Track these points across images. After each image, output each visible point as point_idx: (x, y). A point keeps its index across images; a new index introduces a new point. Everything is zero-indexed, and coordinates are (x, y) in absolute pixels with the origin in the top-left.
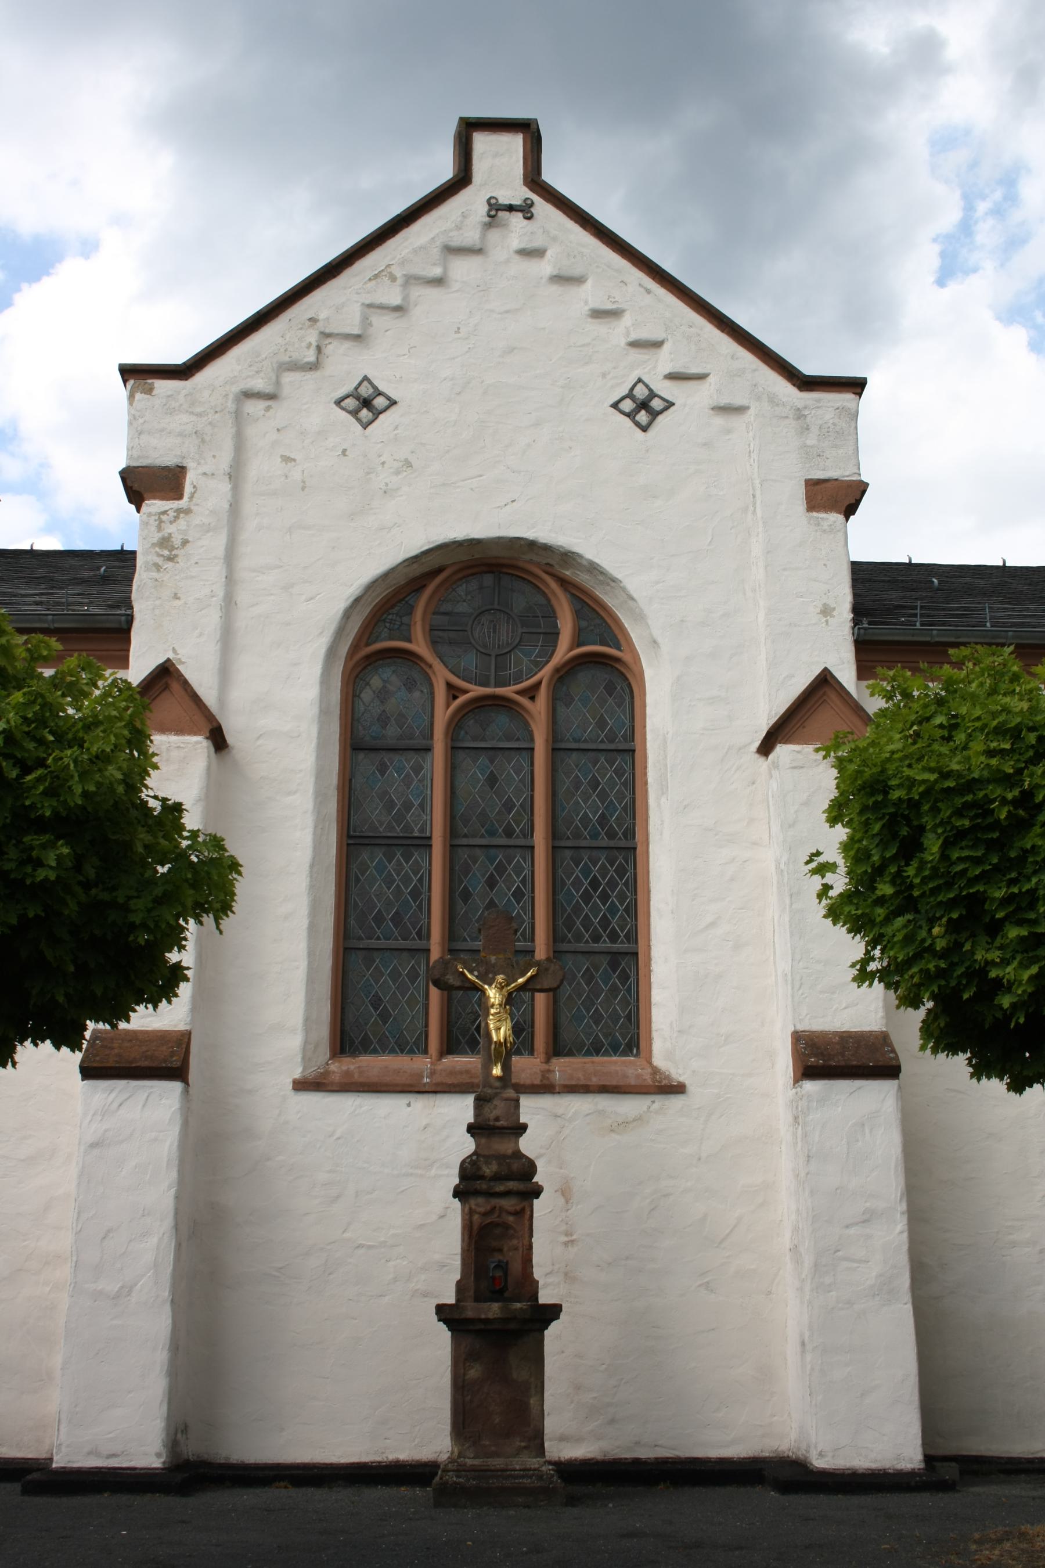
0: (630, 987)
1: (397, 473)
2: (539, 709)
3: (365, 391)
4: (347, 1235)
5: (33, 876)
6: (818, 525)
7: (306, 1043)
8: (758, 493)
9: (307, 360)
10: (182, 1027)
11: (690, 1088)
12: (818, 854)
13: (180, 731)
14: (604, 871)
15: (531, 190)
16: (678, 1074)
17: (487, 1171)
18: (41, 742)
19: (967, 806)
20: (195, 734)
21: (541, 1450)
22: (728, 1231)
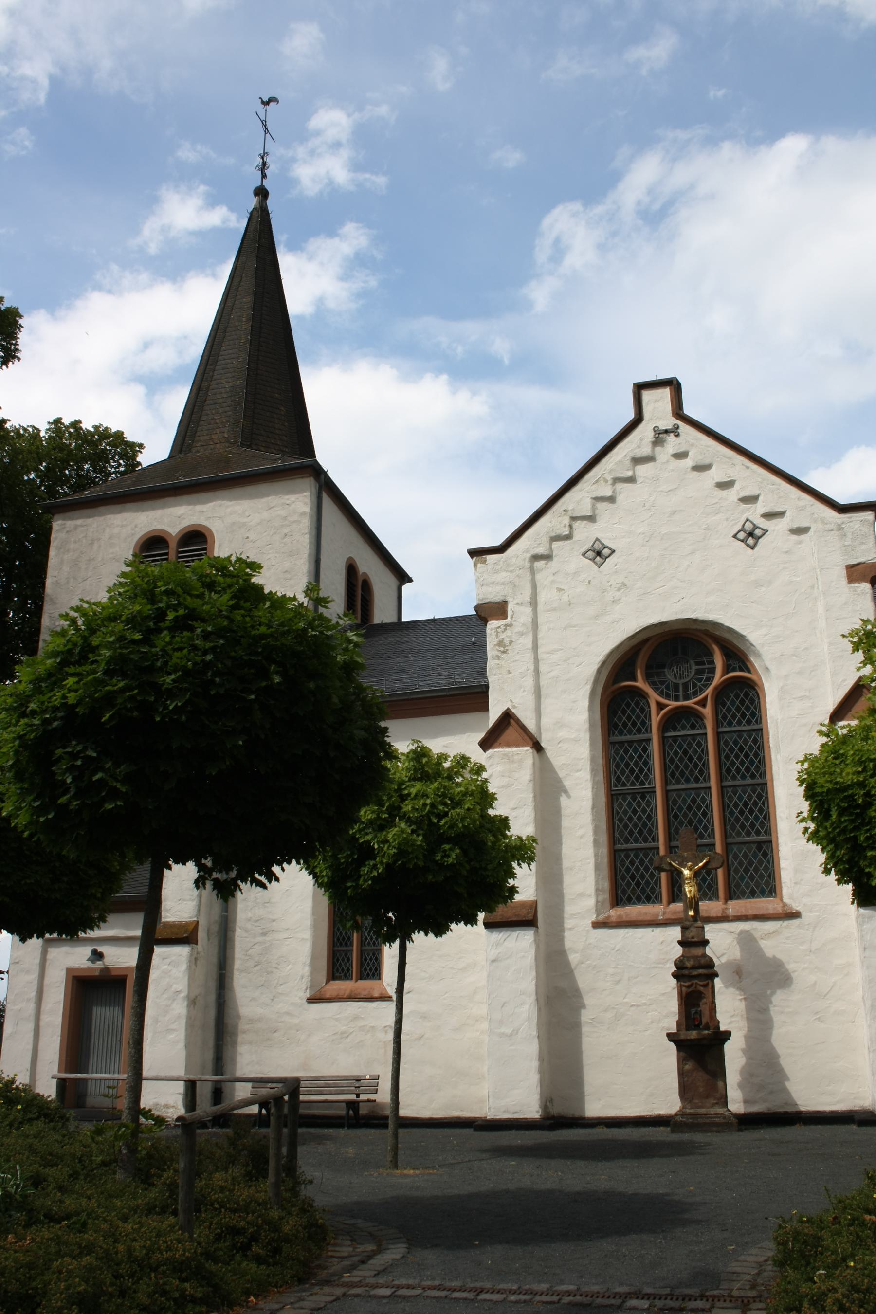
0: (769, 860)
1: (619, 590)
2: (707, 711)
3: (598, 546)
4: (626, 1000)
5: (447, 862)
6: (855, 591)
7: (597, 902)
8: (819, 577)
9: (565, 533)
10: (533, 898)
11: (803, 914)
12: (801, 813)
13: (517, 745)
14: (750, 796)
15: (677, 419)
16: (796, 906)
17: (688, 964)
18: (445, 804)
19: (845, 797)
20: (526, 746)
21: (725, 1104)
22: (828, 989)
